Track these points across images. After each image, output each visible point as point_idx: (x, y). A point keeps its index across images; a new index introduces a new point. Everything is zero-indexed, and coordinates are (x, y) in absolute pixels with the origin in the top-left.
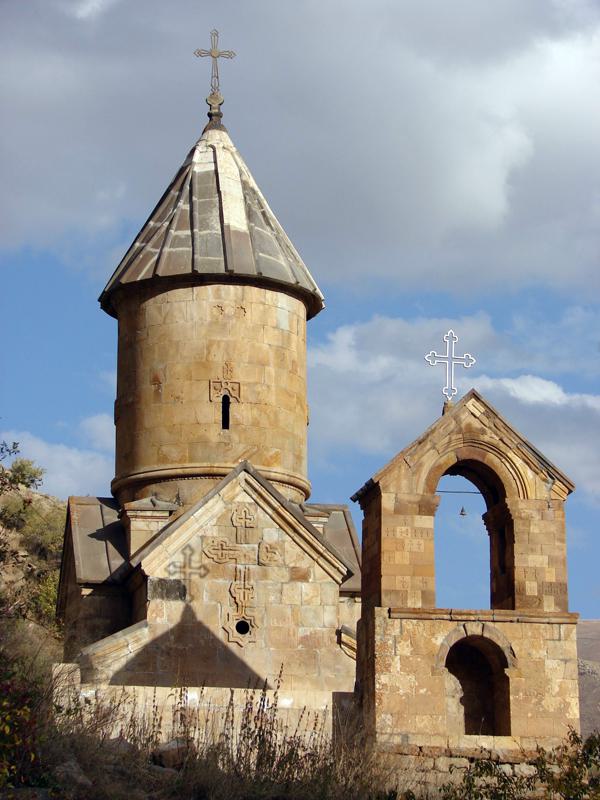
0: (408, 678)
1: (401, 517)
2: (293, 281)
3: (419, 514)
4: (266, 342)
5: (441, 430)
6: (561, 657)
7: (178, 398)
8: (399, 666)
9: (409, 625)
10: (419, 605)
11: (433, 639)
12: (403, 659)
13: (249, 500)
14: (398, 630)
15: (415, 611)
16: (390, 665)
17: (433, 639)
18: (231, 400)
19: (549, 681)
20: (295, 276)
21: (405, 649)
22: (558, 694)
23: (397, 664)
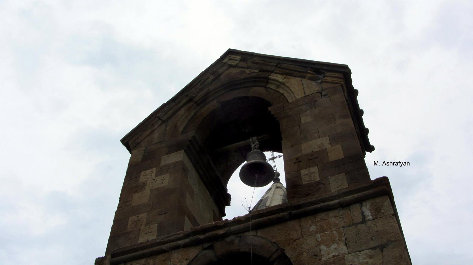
6: (372, 244)
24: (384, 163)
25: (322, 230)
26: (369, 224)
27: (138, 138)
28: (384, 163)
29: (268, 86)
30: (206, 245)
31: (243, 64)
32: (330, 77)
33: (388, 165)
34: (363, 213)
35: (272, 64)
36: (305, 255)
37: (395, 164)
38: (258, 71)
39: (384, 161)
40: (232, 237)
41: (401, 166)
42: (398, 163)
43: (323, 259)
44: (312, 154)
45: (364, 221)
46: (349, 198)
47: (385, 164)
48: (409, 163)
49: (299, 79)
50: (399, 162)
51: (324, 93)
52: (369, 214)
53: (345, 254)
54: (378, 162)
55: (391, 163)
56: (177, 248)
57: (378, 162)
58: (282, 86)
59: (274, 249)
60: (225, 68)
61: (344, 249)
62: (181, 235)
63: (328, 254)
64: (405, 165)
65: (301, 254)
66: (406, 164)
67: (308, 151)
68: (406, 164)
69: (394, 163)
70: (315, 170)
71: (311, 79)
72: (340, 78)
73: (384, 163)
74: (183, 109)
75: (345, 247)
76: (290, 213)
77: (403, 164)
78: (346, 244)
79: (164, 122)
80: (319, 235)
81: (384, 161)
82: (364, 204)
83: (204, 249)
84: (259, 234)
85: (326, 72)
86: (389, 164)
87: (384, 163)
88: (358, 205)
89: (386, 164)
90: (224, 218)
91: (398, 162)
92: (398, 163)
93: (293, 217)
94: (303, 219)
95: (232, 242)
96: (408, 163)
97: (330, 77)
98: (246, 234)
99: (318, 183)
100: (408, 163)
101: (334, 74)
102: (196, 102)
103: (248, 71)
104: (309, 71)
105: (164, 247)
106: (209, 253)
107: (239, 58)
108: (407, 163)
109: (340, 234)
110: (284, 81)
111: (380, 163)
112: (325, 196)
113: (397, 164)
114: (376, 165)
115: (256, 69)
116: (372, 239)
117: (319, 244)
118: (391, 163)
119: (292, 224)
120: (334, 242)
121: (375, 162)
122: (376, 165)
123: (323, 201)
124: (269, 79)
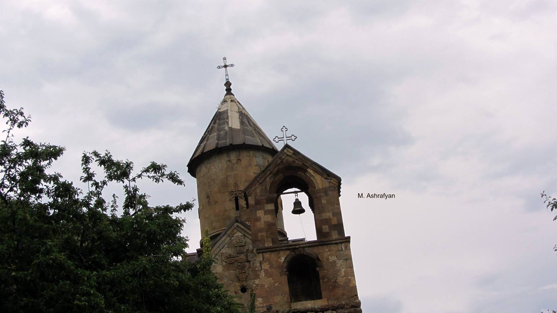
0: (269, 279)
1: (259, 206)
2: (261, 145)
3: (267, 204)
4: (252, 172)
5: (273, 164)
6: (344, 258)
7: (217, 201)
8: (264, 275)
9: (267, 255)
10: (271, 245)
11: (279, 260)
12: (266, 271)
13: (240, 234)
14: (262, 258)
15: (268, 248)
16: (259, 275)
17: (279, 260)
18: (239, 198)
19: (339, 270)
20: (261, 142)
21: (266, 266)
22: (345, 276)
23: (262, 274)
24: (368, 195)
25: (329, 251)
26: (343, 251)
27: (249, 191)
28: (368, 195)
29: (306, 173)
30: (292, 250)
31: (293, 156)
32: (334, 181)
33: (372, 197)
34: (342, 247)
35: (309, 163)
36: (325, 259)
37: (379, 196)
38: (301, 164)
39: (369, 194)
40: (301, 249)
41: (386, 199)
42: (383, 196)
43: (330, 261)
44: (326, 219)
45: (342, 250)
46: (338, 241)
47: (370, 196)
48: (394, 195)
49: (320, 176)
50: (384, 195)
51: (331, 189)
52: (344, 249)
53: (336, 260)
54: (362, 194)
55: (376, 196)
56: (282, 250)
57: (362, 194)
58: (313, 177)
59: (315, 255)
60: (285, 155)
61: (336, 259)
62: (283, 246)
63: (331, 259)
64: (389, 197)
65: (323, 258)
66: (391, 196)
67: (325, 218)
68: (391, 196)
69: (378, 195)
70: (327, 227)
71: (326, 178)
72: (336, 182)
73: (369, 195)
74: (268, 177)
75: (336, 258)
76: (320, 244)
77: (388, 196)
78: (336, 257)
79: (260, 183)
80: (329, 253)
81: (369, 194)
82: (342, 244)
83: (291, 251)
84: (310, 249)
85: (332, 177)
86: (374, 196)
87: (369, 195)
88: (340, 244)
89: (371, 196)
90: (37, 185)
91: (383, 194)
92: (383, 196)
93: (320, 245)
94: (324, 246)
95: (301, 250)
96: (393, 196)
97: (334, 181)
98: (305, 248)
99: (328, 233)
100: (393, 196)
101: (335, 180)
102: (273, 174)
103: (297, 161)
104: (325, 174)
105: (278, 249)
106: (293, 253)
107: (292, 152)
108: (392, 195)
109: (335, 253)
110: (314, 175)
111: (365, 195)
112: (331, 239)
113: (382, 196)
114: (360, 197)
115: (301, 162)
116: (344, 256)
117: (329, 256)
118: (376, 196)
119: (320, 247)
120: (333, 256)
121: (359, 194)
122: (360, 197)
123: (331, 241)
124: (306, 170)
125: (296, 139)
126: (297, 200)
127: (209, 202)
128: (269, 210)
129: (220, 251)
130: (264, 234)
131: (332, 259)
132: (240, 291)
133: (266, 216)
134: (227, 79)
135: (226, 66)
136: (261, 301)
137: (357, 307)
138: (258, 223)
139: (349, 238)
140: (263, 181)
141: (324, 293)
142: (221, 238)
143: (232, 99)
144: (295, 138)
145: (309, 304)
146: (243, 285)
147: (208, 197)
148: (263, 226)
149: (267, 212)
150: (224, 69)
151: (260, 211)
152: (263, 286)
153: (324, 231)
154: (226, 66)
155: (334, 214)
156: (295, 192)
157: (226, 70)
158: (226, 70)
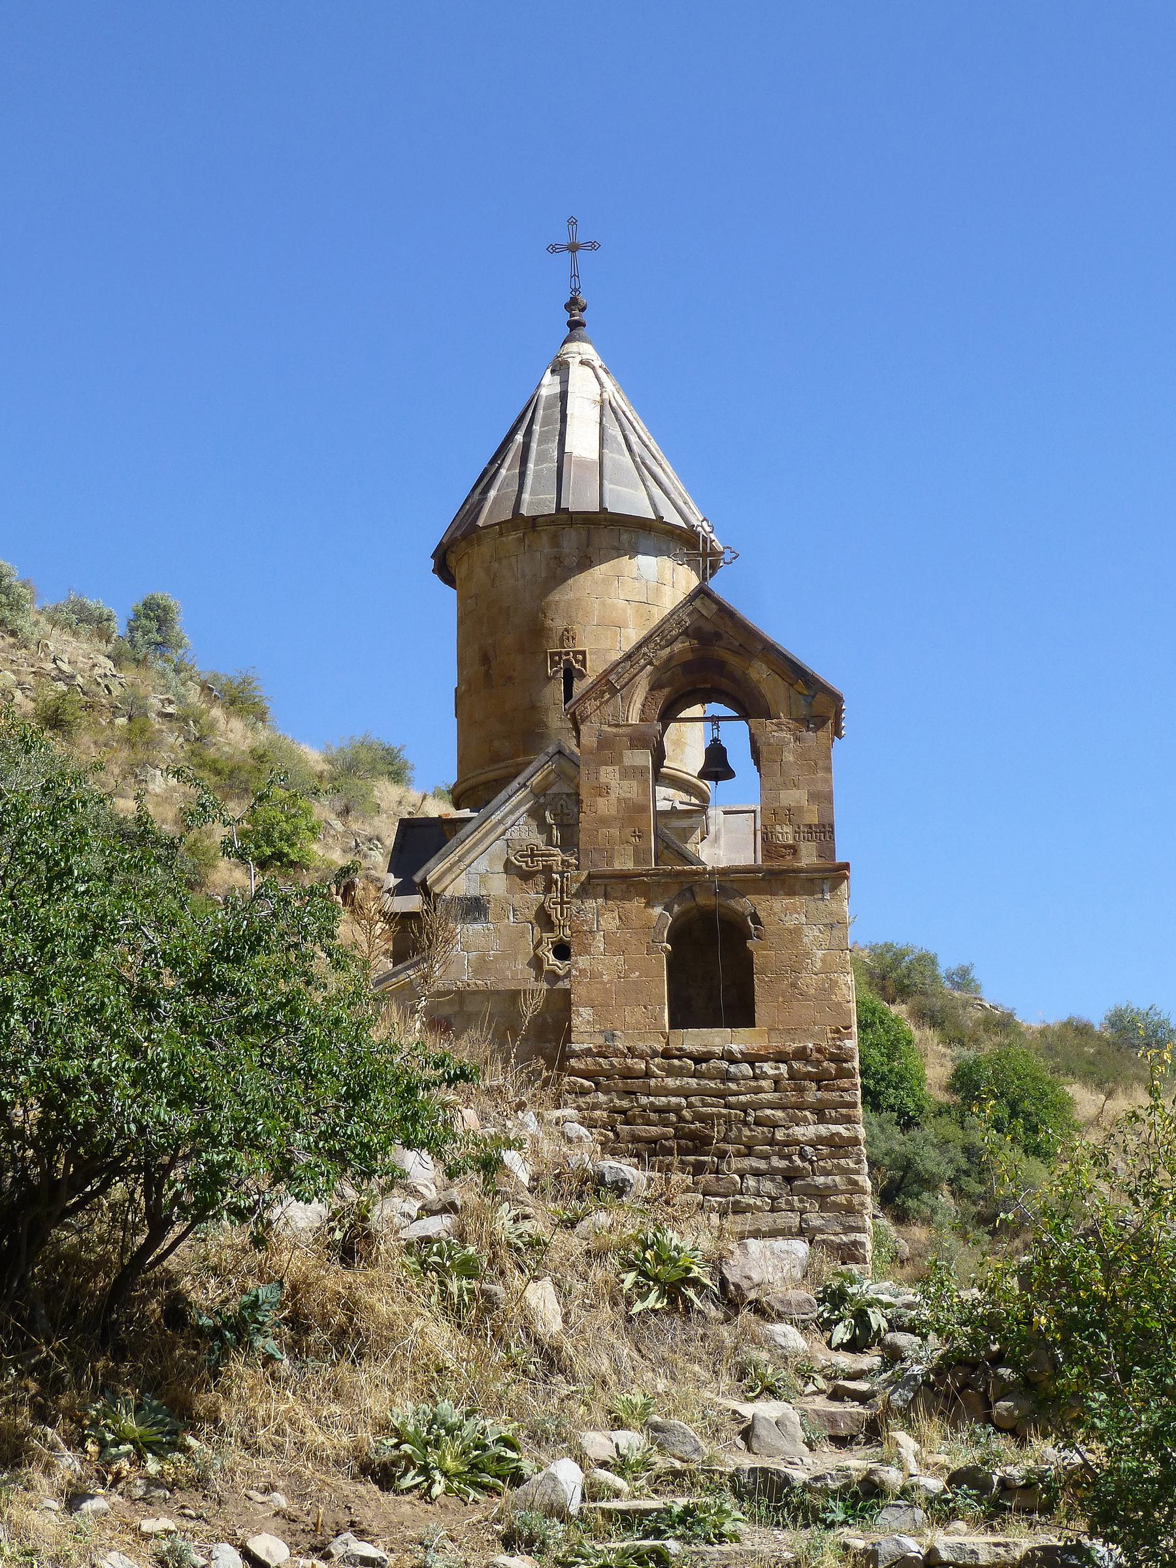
0: (615, 959)
6: (826, 921)
7: (510, 678)
21: (610, 922)
23: (599, 943)
70: (787, 829)
125: (734, 558)
126: (715, 740)
127: (487, 674)
128: (634, 768)
129: (504, 833)
130: (615, 832)
131: (791, 921)
132: (551, 956)
133: (625, 783)
134: (575, 290)
135: (573, 248)
136: (587, 1017)
137: (846, 1061)
138: (600, 801)
139: (846, 866)
140: (627, 684)
141: (761, 1011)
142: (511, 797)
143: (584, 357)
144: (734, 555)
145: (717, 1039)
146: (561, 939)
147: (485, 659)
148: (613, 812)
149: (628, 773)
150: (568, 254)
151: (610, 769)
152: (595, 976)
153: (782, 840)
154: (573, 248)
155: (814, 797)
156: (715, 720)
157: (574, 261)
158: (574, 261)
